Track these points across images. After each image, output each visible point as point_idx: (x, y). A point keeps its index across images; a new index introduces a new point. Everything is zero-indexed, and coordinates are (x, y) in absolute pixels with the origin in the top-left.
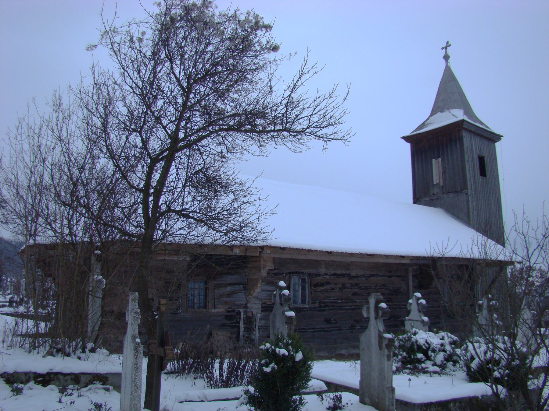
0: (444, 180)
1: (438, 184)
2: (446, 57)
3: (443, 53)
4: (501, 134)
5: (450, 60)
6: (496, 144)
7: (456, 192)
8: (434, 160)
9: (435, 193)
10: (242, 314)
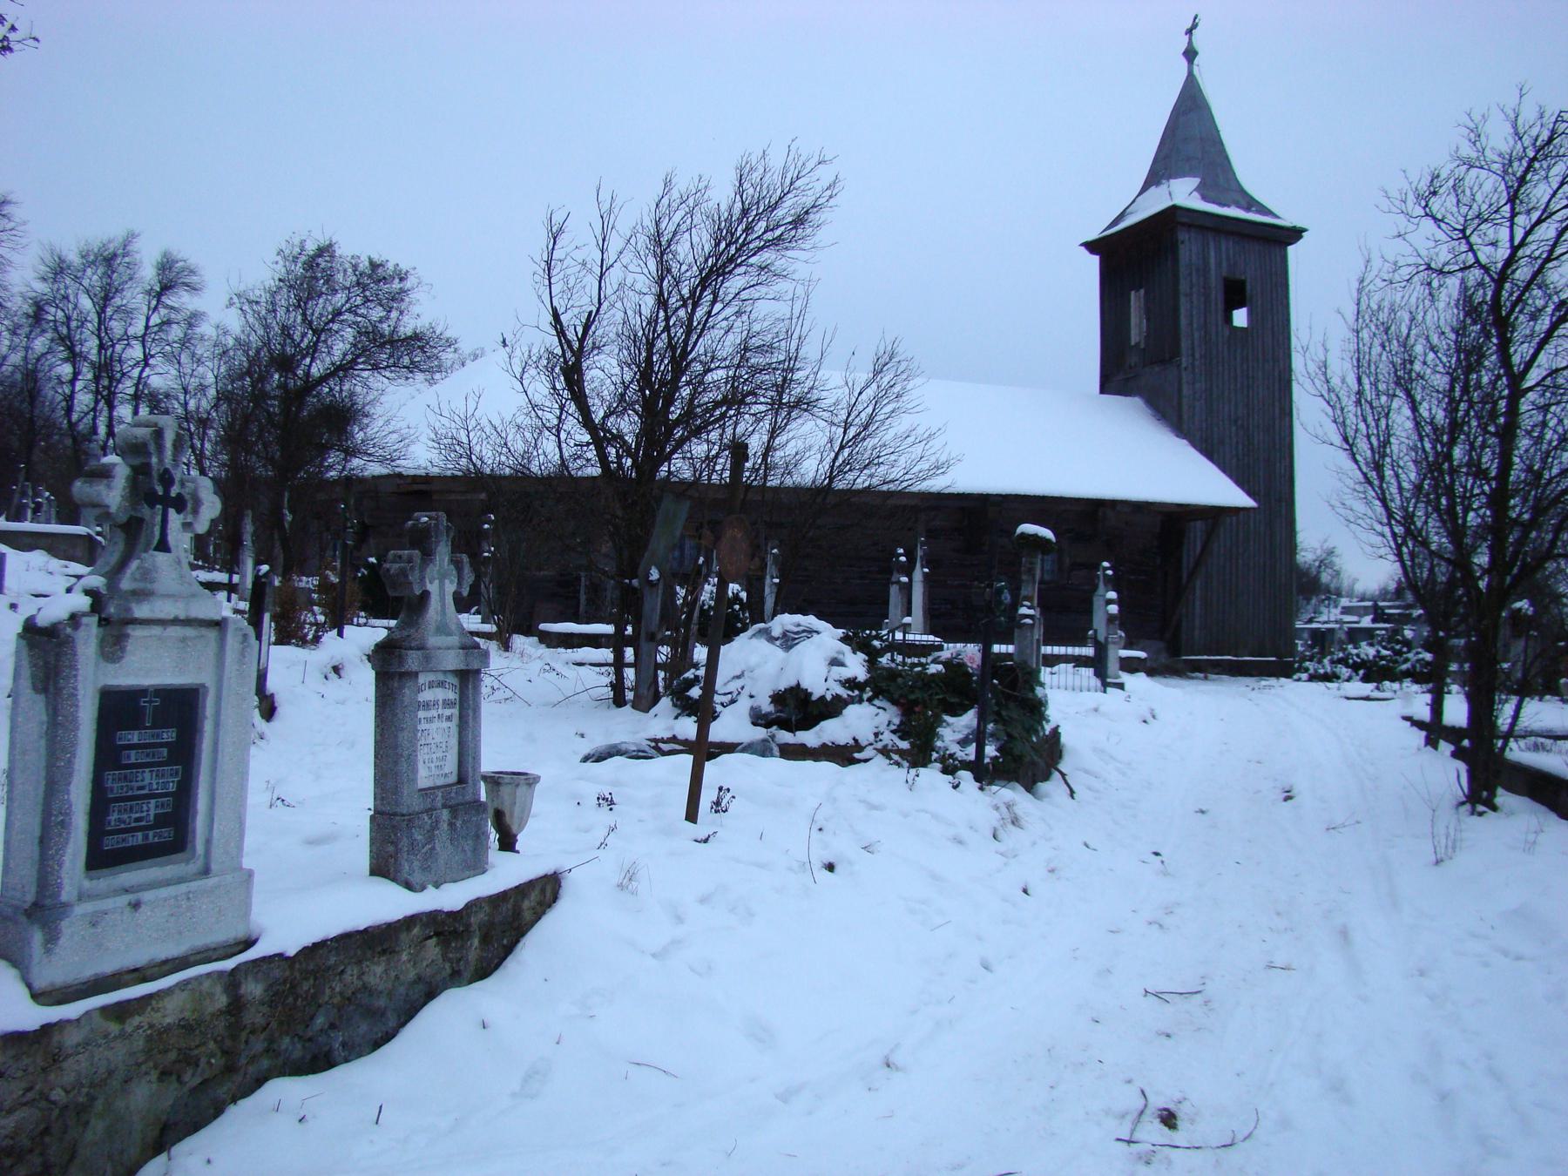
1: (1137, 344)
2: (1190, 54)
3: (1183, 43)
4: (1299, 224)
6: (1291, 249)
8: (1133, 293)
10: (583, 579)
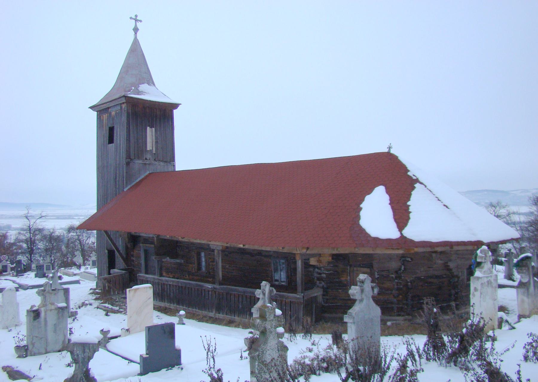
0: (157, 149)
1: (151, 151)
2: (136, 30)
5: (138, 33)
7: (166, 162)
8: (148, 128)
9: (148, 158)
